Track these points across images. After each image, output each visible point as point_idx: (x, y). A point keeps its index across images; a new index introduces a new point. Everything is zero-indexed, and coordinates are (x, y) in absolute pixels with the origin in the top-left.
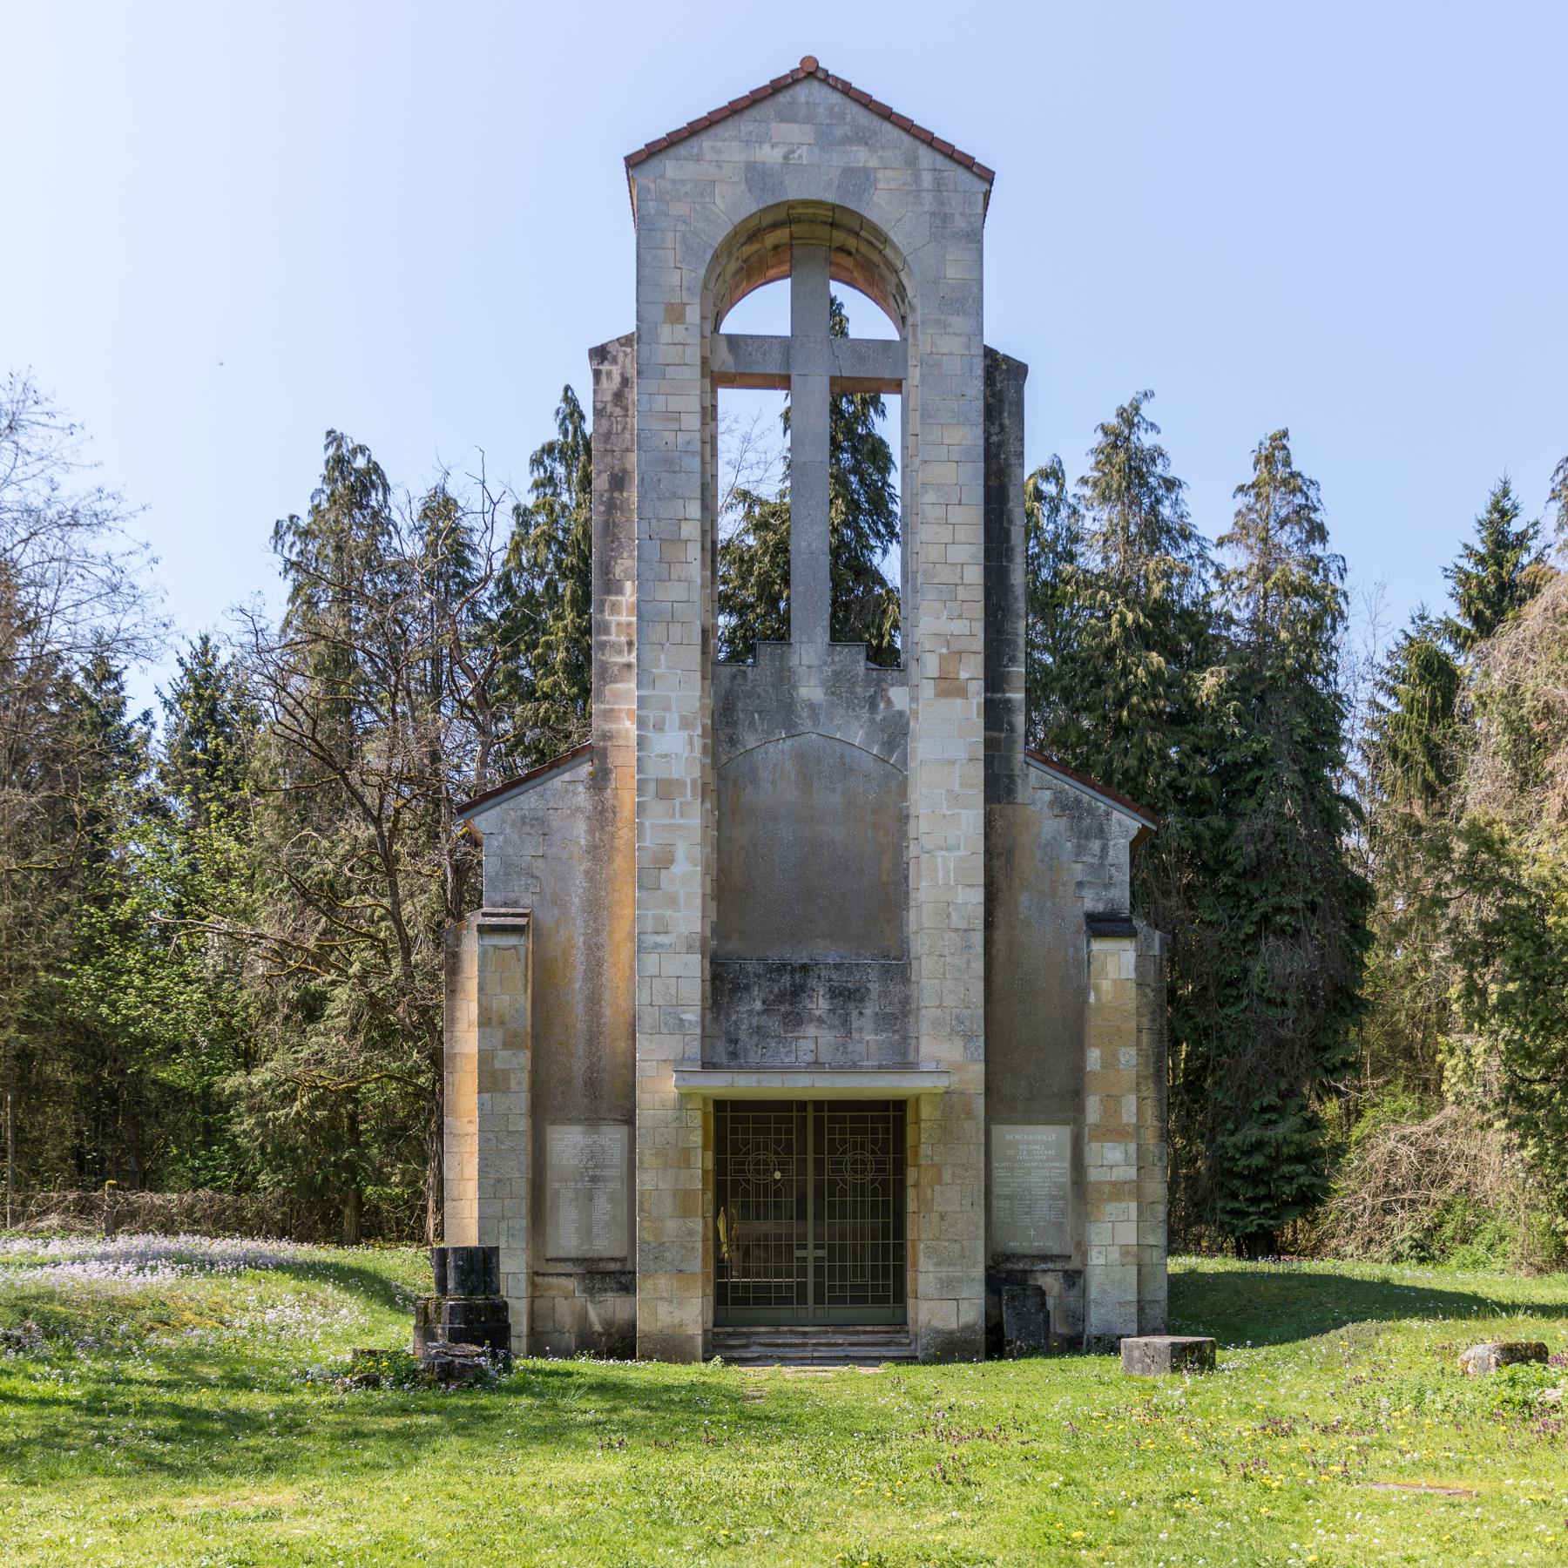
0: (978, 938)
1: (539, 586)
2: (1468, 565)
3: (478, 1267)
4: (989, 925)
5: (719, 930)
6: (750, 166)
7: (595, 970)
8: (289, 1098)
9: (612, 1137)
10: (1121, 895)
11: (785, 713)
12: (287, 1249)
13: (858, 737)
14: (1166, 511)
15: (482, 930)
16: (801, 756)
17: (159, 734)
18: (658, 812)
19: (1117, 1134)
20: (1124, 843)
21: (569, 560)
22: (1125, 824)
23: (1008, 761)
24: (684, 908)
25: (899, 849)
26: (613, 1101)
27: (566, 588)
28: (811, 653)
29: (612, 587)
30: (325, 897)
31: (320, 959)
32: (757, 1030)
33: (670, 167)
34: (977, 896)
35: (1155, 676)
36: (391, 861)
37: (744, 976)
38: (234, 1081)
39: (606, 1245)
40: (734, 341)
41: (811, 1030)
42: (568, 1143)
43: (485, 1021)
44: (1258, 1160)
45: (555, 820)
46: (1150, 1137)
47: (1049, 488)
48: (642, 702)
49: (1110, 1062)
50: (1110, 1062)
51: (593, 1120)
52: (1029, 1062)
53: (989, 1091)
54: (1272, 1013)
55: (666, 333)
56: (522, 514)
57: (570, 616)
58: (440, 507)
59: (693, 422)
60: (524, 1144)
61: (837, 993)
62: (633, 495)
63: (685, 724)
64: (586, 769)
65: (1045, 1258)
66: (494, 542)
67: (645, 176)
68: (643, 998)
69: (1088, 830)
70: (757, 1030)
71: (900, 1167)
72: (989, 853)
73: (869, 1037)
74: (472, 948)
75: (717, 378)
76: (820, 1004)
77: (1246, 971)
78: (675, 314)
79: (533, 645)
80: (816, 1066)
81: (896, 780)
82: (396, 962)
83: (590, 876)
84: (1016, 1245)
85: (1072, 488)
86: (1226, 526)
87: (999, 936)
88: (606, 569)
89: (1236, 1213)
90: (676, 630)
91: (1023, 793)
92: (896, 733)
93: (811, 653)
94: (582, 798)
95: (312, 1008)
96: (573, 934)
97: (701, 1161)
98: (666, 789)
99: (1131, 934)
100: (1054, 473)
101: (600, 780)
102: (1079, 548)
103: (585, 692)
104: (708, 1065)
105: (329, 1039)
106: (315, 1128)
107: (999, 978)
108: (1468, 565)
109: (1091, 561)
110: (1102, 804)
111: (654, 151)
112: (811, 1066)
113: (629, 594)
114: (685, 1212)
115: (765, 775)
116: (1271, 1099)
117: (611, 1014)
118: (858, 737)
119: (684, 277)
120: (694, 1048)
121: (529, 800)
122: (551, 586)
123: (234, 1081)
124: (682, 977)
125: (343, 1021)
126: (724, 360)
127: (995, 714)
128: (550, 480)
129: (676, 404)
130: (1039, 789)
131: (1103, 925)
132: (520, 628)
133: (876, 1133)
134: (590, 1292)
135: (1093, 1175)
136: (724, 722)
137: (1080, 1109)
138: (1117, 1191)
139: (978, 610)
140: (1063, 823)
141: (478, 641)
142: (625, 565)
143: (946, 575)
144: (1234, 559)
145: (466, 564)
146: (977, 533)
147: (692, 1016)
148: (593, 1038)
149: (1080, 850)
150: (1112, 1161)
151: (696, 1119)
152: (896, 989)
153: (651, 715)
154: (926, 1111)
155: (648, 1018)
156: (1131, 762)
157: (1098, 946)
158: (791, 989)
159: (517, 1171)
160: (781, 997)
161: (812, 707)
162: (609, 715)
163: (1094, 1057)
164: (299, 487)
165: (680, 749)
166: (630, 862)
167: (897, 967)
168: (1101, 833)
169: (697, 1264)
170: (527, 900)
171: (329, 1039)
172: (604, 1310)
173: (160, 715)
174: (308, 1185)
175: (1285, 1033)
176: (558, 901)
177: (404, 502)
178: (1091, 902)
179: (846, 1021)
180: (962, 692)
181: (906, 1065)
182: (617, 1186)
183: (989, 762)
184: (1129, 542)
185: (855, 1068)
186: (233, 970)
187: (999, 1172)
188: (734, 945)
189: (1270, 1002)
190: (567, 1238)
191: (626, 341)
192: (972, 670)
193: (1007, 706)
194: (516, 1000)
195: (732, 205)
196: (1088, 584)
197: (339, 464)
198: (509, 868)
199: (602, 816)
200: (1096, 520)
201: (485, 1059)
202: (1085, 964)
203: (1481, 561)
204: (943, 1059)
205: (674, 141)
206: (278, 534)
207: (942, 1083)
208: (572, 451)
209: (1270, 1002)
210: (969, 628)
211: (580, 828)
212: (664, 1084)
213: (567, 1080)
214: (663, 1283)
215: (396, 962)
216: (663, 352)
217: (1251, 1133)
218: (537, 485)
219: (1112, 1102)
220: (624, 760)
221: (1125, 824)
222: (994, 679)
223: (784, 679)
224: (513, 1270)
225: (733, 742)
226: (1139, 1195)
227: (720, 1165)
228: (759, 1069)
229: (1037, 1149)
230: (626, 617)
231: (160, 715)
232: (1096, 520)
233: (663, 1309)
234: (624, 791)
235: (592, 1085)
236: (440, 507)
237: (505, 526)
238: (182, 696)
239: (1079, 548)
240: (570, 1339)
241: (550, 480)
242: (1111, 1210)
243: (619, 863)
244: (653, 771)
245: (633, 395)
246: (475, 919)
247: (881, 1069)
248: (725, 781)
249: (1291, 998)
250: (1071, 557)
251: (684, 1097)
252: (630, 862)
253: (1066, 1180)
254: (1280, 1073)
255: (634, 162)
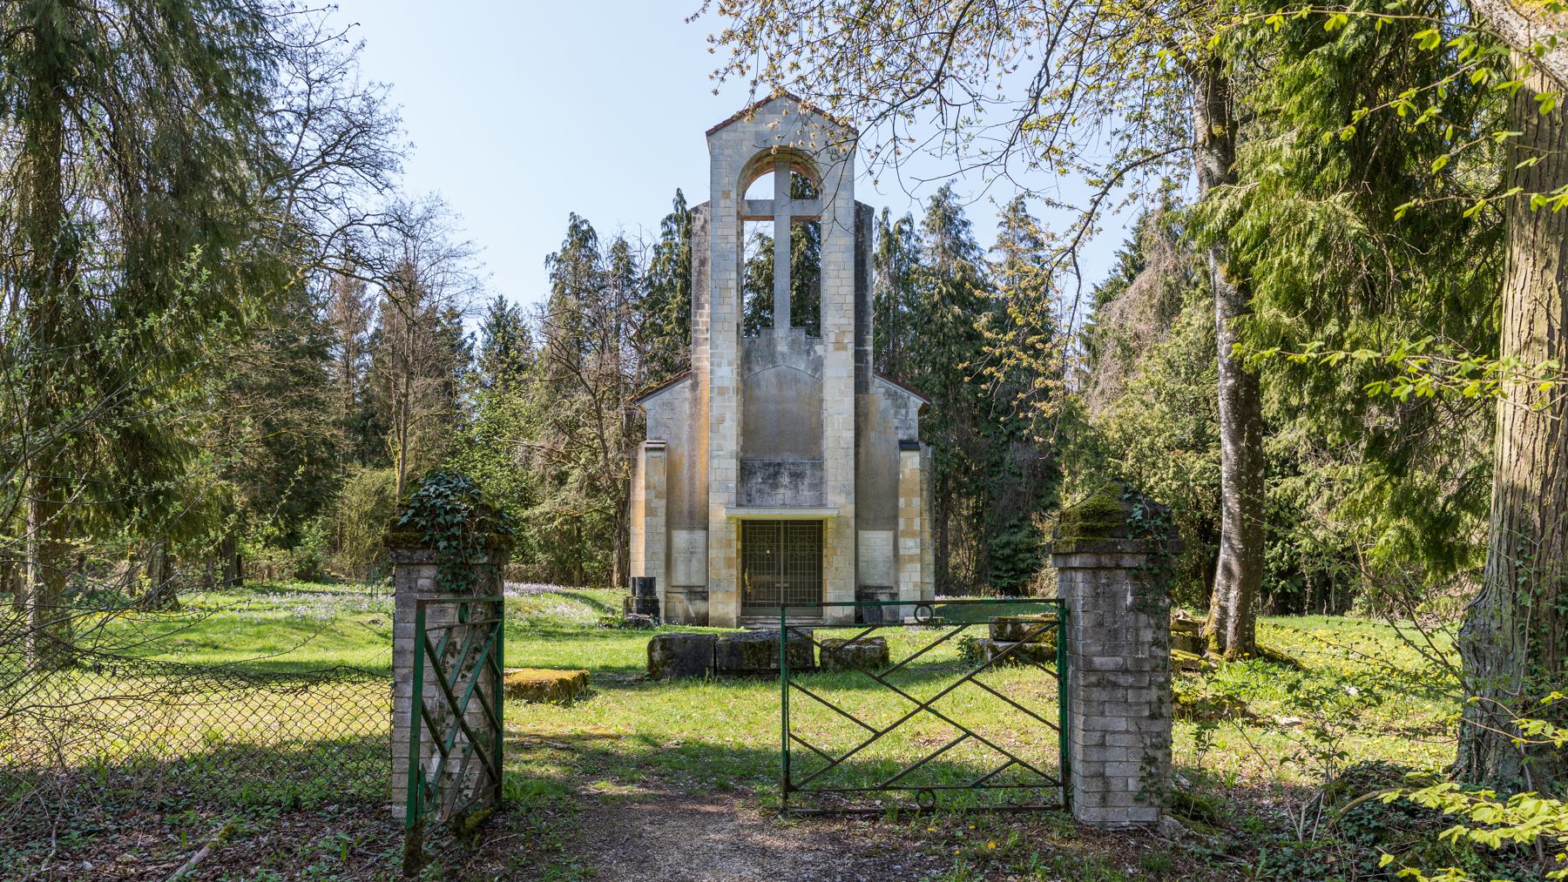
0: (852, 452)
1: (664, 281)
2: (1126, 250)
3: (647, 584)
4: (857, 445)
5: (744, 449)
6: (757, 133)
7: (692, 465)
8: (552, 520)
9: (699, 535)
10: (914, 432)
11: (772, 358)
12: (561, 589)
13: (802, 366)
14: (963, 236)
15: (647, 449)
16: (778, 376)
17: (479, 344)
18: (718, 401)
19: (912, 535)
20: (916, 410)
21: (679, 270)
22: (916, 402)
23: (866, 376)
24: (729, 440)
25: (819, 414)
26: (699, 520)
27: (678, 283)
28: (782, 331)
29: (700, 306)
30: (568, 427)
31: (567, 457)
32: (760, 491)
33: (724, 135)
34: (851, 434)
35: (956, 317)
36: (599, 410)
37: (756, 468)
38: (526, 513)
39: (696, 580)
40: (750, 203)
41: (782, 490)
42: (681, 538)
43: (647, 487)
44: (1007, 551)
45: (676, 403)
46: (927, 536)
47: (906, 228)
48: (712, 355)
49: (908, 504)
50: (908, 504)
51: (691, 528)
52: (875, 504)
53: (857, 516)
54: (1017, 479)
55: (722, 203)
56: (657, 249)
57: (679, 297)
58: (621, 247)
59: (733, 239)
60: (663, 538)
61: (792, 475)
62: (708, 268)
63: (730, 364)
64: (689, 382)
65: (882, 588)
66: (644, 263)
67: (714, 139)
68: (712, 478)
69: (902, 405)
70: (760, 491)
71: (820, 549)
72: (857, 415)
73: (806, 493)
74: (642, 457)
75: (742, 218)
76: (785, 480)
77: (1002, 459)
78: (726, 195)
79: (662, 310)
80: (784, 505)
81: (818, 385)
82: (601, 457)
83: (690, 426)
84: (869, 582)
85: (917, 226)
86: (994, 242)
87: (862, 450)
88: (698, 299)
89: (997, 577)
90: (726, 326)
91: (872, 390)
92: (818, 365)
93: (782, 331)
94: (688, 394)
95: (561, 479)
96: (683, 451)
97: (736, 545)
98: (722, 391)
99: (918, 449)
100: (908, 220)
101: (695, 386)
102: (920, 256)
103: (687, 331)
104: (739, 505)
105: (571, 493)
106: (562, 534)
107: (862, 468)
108: (1126, 250)
109: (926, 261)
110: (906, 393)
111: (717, 129)
112: (781, 506)
113: (707, 309)
114: (729, 567)
115: (763, 383)
116: (1014, 521)
117: (699, 483)
118: (802, 366)
119: (730, 180)
120: (733, 498)
121: (666, 395)
122: (670, 282)
123: (526, 513)
124: (728, 468)
125: (576, 485)
126: (746, 210)
127: (859, 356)
128: (670, 232)
129: (726, 232)
130: (879, 387)
131: (906, 445)
132: (655, 303)
133: (808, 537)
134: (690, 600)
135: (902, 552)
136: (746, 361)
137: (897, 524)
138: (911, 559)
139: (852, 314)
140: (889, 402)
141: (637, 308)
142: (705, 297)
143: (838, 299)
144: (999, 257)
145: (631, 272)
146: (851, 282)
147: (732, 485)
148: (692, 494)
149: (896, 413)
150: (910, 546)
151: (734, 528)
152: (818, 473)
153: (716, 360)
154: (830, 525)
155: (714, 486)
156: (944, 360)
157: (903, 454)
158: (773, 473)
159: (660, 548)
160: (769, 477)
161: (783, 354)
162: (698, 359)
163: (902, 501)
164: (557, 239)
165: (728, 374)
166: (705, 420)
167: (818, 464)
168: (906, 406)
169: (734, 588)
170: (665, 437)
171: (571, 493)
172: (696, 607)
173: (479, 335)
174: (559, 560)
175: (1021, 489)
176: (678, 437)
177: (604, 246)
178: (902, 435)
179: (796, 486)
180: (845, 348)
181: (822, 505)
182: (701, 556)
183: (857, 376)
184: (944, 251)
185: (800, 506)
186: (527, 462)
187: (862, 550)
188: (750, 455)
189: (1014, 474)
190: (680, 578)
191: (706, 205)
192: (849, 339)
193: (865, 353)
194: (660, 478)
195: (749, 150)
196: (925, 274)
197: (575, 228)
198: (658, 424)
199: (696, 401)
200: (929, 241)
201: (648, 502)
202: (898, 462)
203: (1133, 248)
204: (837, 503)
205: (726, 124)
206: (547, 261)
207: (835, 513)
208: (683, 218)
209: (1014, 474)
210: (848, 322)
211: (687, 406)
212: (722, 513)
213: (683, 513)
214: (720, 595)
215: (601, 457)
216: (721, 211)
217: (1004, 538)
218: (664, 234)
219: (910, 520)
220: (704, 378)
221: (916, 402)
222: (859, 341)
223: (771, 343)
224: (660, 589)
225: (750, 369)
226: (922, 560)
227: (744, 548)
228: (760, 506)
229: (877, 541)
230: (706, 319)
231: (479, 335)
232: (929, 241)
233: (720, 607)
234: (705, 391)
235: (691, 514)
236: (621, 247)
237: (651, 254)
238: (490, 326)
239: (920, 256)
240: (682, 619)
241: (670, 232)
242: (909, 566)
243: (702, 421)
244: (717, 383)
245: (709, 227)
246: (644, 445)
247: (811, 507)
248: (747, 387)
249: (1024, 472)
250: (916, 261)
251: (729, 518)
252: (705, 420)
253: (891, 554)
254: (1019, 508)
255: (709, 134)
